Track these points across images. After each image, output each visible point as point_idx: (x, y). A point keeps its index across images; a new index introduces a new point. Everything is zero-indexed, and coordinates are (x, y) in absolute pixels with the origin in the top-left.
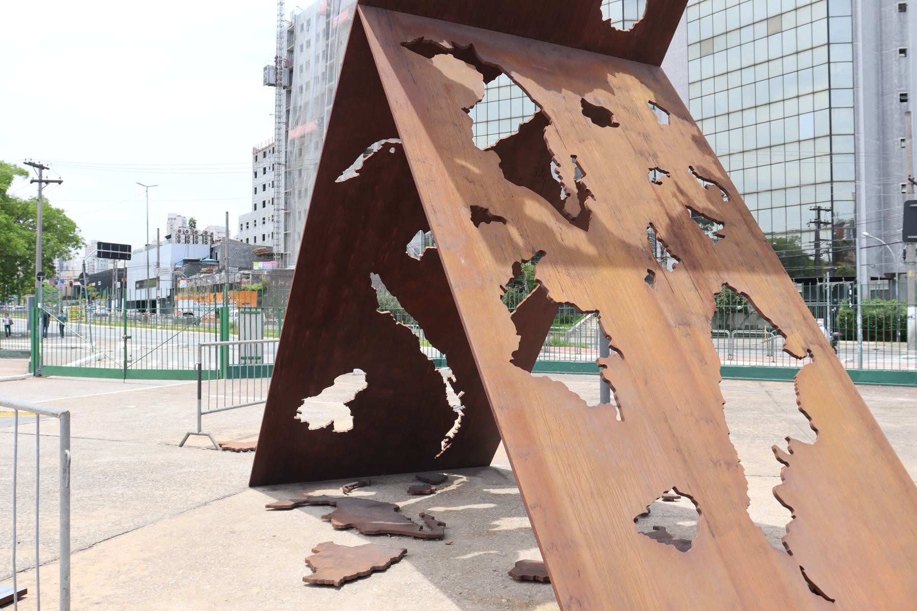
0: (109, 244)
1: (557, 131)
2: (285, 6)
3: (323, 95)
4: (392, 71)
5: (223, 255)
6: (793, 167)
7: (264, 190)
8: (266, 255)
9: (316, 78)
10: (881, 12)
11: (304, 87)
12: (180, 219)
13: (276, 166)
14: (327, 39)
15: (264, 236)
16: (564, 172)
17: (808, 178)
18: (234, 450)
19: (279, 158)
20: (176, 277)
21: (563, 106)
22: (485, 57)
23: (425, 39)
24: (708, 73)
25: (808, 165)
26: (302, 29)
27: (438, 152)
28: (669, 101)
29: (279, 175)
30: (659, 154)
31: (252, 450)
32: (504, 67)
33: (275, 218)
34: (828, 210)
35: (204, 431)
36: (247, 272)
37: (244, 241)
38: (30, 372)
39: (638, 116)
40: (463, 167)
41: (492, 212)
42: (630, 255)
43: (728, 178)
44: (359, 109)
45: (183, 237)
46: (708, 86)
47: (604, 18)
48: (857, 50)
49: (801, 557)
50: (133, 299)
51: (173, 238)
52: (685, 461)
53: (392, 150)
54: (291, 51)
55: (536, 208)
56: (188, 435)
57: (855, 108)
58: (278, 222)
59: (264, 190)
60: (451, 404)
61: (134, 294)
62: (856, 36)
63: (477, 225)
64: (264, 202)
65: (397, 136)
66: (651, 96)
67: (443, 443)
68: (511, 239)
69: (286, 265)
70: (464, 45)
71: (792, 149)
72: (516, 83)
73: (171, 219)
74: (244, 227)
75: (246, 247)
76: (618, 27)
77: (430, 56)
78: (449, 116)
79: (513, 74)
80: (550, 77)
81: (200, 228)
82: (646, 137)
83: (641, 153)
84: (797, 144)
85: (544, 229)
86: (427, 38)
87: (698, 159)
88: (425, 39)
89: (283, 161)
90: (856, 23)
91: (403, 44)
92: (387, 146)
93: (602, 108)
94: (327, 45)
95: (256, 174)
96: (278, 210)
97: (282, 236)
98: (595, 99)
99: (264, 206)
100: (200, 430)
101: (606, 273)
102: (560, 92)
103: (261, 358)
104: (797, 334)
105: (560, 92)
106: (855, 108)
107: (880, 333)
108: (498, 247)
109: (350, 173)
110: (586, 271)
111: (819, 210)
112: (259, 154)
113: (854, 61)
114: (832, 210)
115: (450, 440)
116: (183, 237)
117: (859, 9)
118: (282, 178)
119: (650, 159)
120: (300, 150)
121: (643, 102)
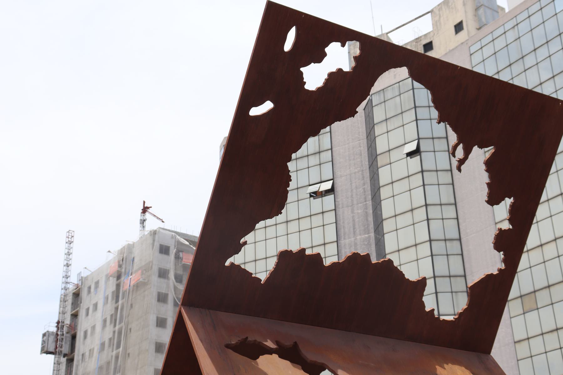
3: (108, 363)
9: (103, 345)
11: (87, 354)
14: (117, 301)
22: (310, 356)
23: (249, 339)
47: (428, 309)
54: (75, 316)
70: (288, 343)
77: (255, 357)
88: (249, 339)
91: (228, 346)
94: (117, 309)
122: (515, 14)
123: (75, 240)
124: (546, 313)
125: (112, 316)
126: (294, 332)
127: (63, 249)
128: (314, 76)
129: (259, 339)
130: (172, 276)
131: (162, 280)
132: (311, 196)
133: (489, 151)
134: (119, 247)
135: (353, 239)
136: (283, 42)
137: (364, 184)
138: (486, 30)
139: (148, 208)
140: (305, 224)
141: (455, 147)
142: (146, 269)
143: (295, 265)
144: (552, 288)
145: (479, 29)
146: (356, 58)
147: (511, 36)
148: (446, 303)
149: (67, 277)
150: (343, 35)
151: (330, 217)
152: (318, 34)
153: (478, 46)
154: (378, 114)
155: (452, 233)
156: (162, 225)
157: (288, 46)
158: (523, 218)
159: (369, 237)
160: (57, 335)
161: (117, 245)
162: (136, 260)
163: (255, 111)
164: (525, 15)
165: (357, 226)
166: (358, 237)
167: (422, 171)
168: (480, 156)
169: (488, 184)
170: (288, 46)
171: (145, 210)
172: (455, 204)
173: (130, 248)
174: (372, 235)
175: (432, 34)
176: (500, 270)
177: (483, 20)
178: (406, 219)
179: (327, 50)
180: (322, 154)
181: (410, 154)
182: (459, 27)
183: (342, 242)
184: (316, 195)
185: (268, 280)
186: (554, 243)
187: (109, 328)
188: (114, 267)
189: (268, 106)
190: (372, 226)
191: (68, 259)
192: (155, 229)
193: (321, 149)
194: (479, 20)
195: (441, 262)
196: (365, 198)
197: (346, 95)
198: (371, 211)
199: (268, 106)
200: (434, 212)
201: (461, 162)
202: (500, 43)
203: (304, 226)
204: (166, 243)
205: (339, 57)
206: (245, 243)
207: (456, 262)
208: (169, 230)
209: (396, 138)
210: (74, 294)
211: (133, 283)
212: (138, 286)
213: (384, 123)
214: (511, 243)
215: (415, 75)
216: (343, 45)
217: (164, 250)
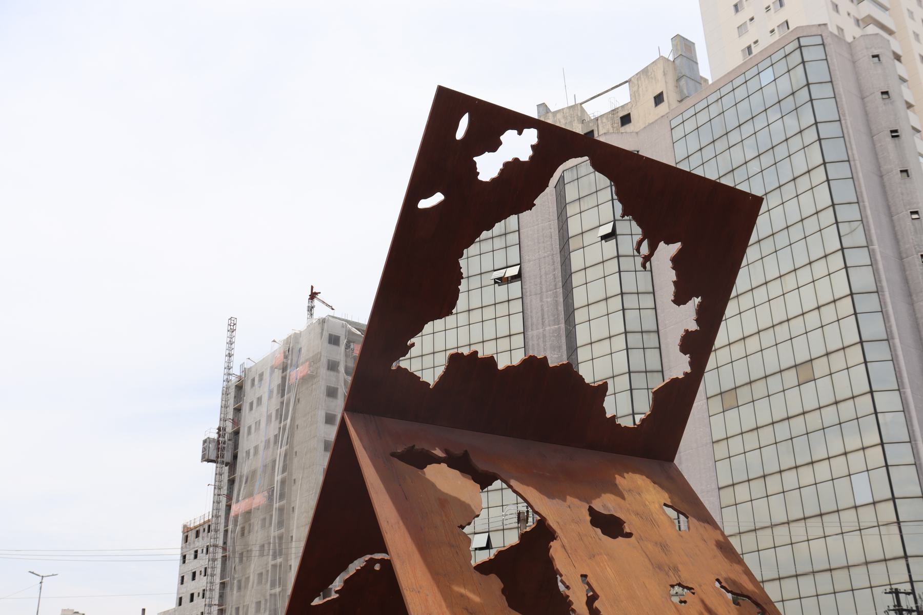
1: (564, 547)
2: (234, 358)
4: (382, 486)
6: (853, 540)
7: (194, 578)
9: (268, 442)
11: (252, 452)
13: (211, 549)
14: (283, 396)
19: (216, 538)
21: (567, 516)
22: (482, 465)
23: (417, 447)
24: (734, 429)
27: (434, 578)
28: (687, 502)
29: (214, 560)
30: (680, 567)
34: (908, 594)
40: (462, 596)
43: (762, 590)
46: (736, 445)
47: (608, 415)
48: (906, 399)
54: (238, 410)
59: (194, 578)
62: (902, 382)
64: (192, 595)
65: (385, 550)
66: (665, 497)
70: (458, 452)
71: (849, 517)
76: (626, 422)
78: (440, 529)
79: (513, 483)
80: (552, 483)
82: (664, 547)
83: (660, 567)
84: (854, 511)
86: (418, 446)
87: (726, 569)
88: (417, 447)
89: (220, 543)
90: (899, 368)
91: (393, 455)
92: (372, 562)
93: (612, 515)
94: (282, 403)
95: (184, 557)
96: (210, 606)
98: (604, 506)
99: (192, 600)
102: (564, 500)
105: (564, 500)
111: (897, 593)
112: (190, 533)
113: (905, 410)
114: (913, 592)
117: (900, 353)
118: (219, 564)
119: (671, 573)
120: (243, 529)
121: (657, 506)
122: (718, 86)
123: (238, 327)
124: (746, 411)
125: (277, 410)
126: (465, 440)
127: (224, 352)
128: (488, 166)
129: (426, 447)
130: (342, 368)
131: (332, 373)
132: (496, 282)
133: (676, 247)
134: (285, 337)
135: (541, 330)
136: (457, 126)
137: (554, 270)
138: (688, 103)
139: (316, 294)
140: (489, 313)
141: (640, 243)
142: (315, 360)
143: (467, 368)
144: (753, 385)
145: (680, 101)
146: (533, 147)
147: (715, 110)
148: (626, 406)
149: (229, 368)
150: (520, 122)
151: (517, 306)
152: (493, 122)
153: (679, 119)
154: (571, 193)
155: (650, 325)
156: (331, 313)
157: (460, 134)
158: (710, 318)
159: (559, 328)
160: (218, 441)
161: (283, 335)
162: (303, 351)
163: (424, 204)
164: (729, 88)
165: (546, 316)
166: (548, 328)
167: (618, 256)
168: (667, 251)
169: (674, 282)
170: (460, 134)
171: (313, 296)
172: (654, 293)
173: (296, 337)
174: (563, 326)
175: (630, 106)
176: (686, 374)
177: (685, 91)
178: (601, 308)
179: (502, 138)
180: (508, 236)
181: (605, 237)
182: (659, 99)
183: (530, 333)
184: (501, 281)
185: (437, 384)
186: (757, 336)
188: (280, 358)
189: (438, 198)
190: (562, 316)
192: (324, 317)
193: (508, 231)
194: (681, 92)
195: (636, 356)
196: (556, 285)
197: (521, 187)
198: (562, 300)
199: (438, 198)
200: (631, 301)
201: (647, 259)
202: (703, 118)
203: (488, 319)
204: (336, 332)
205: (518, 146)
206: (413, 345)
207: (653, 355)
208: (339, 319)
209: (590, 219)
211: (300, 375)
212: (306, 379)
213: (577, 203)
214: (698, 345)
215: (598, 166)
216: (520, 133)
217: (334, 340)
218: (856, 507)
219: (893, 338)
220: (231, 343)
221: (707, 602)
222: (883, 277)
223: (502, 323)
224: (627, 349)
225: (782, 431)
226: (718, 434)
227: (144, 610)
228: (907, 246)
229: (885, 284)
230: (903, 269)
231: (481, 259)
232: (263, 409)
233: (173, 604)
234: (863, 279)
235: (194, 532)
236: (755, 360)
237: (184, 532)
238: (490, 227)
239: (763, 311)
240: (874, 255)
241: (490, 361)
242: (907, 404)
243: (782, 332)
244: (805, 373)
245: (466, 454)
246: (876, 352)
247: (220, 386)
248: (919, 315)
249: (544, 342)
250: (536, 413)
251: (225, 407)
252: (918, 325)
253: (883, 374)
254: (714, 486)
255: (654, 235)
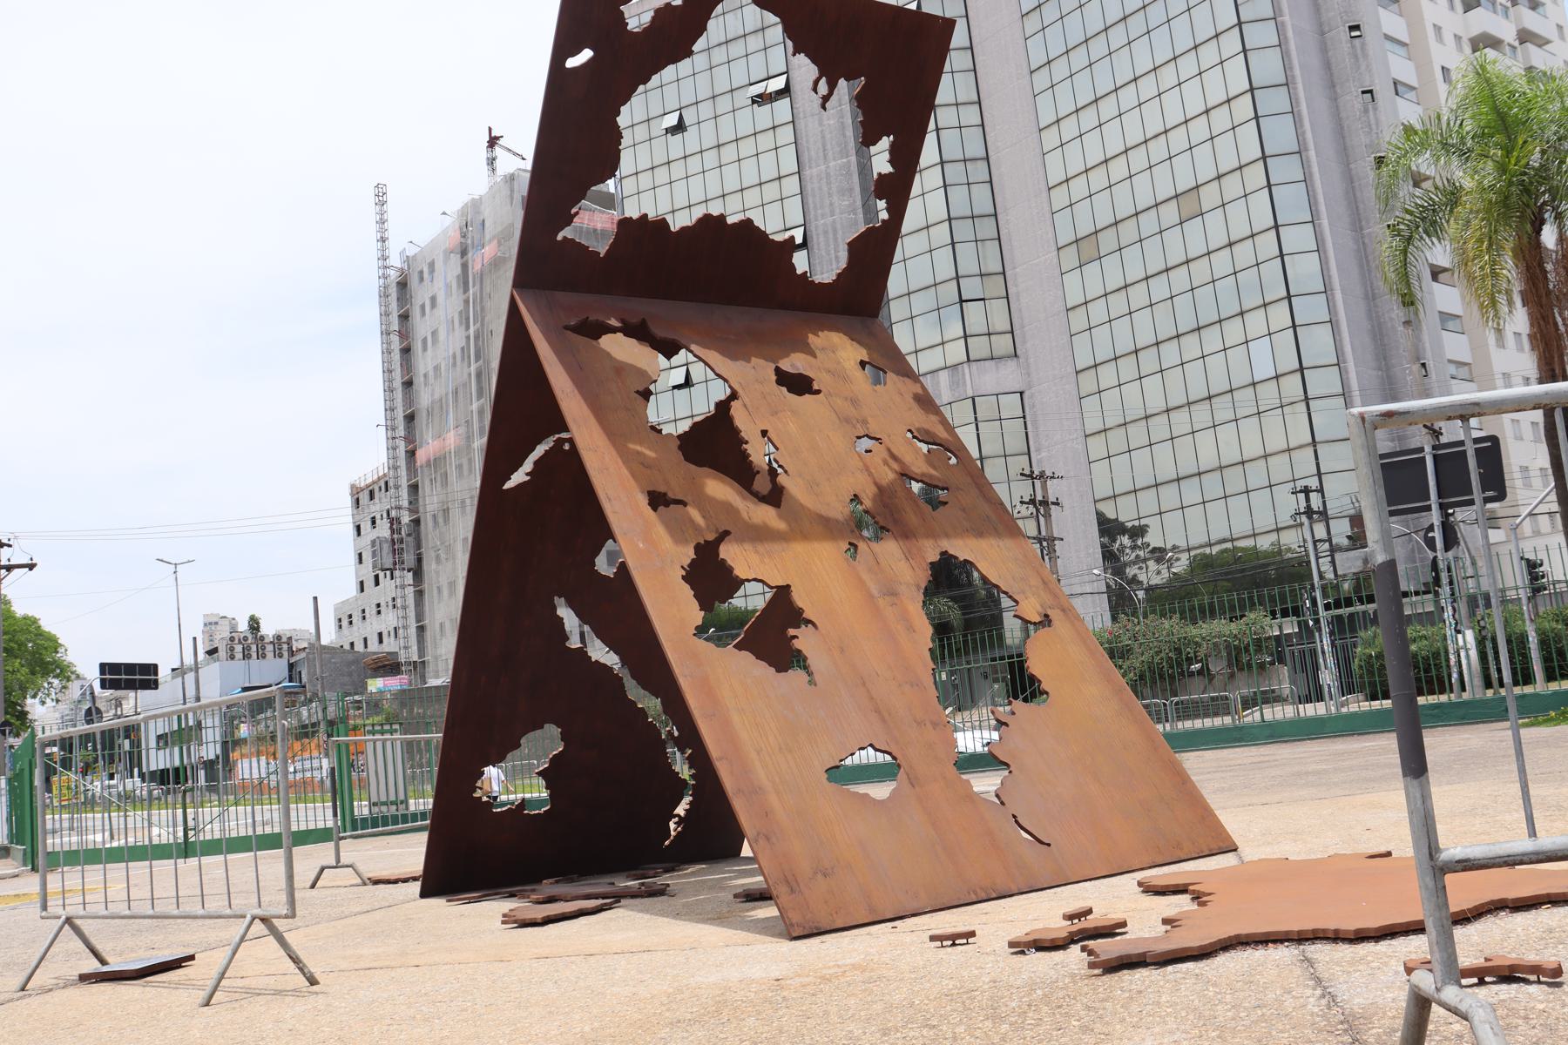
0: (119, 665)
5: (311, 674)
8: (389, 666)
10: (1350, 170)
12: (226, 622)
14: (466, 290)
15: (380, 635)
16: (759, 453)
17: (1276, 442)
18: (389, 882)
20: (233, 718)
21: (753, 376)
22: (659, 332)
24: (1095, 289)
25: (1273, 421)
26: (422, 279)
28: (887, 360)
31: (415, 879)
32: (683, 342)
33: (399, 602)
35: (343, 861)
36: (357, 698)
37: (347, 647)
38: (25, 864)
39: (845, 378)
41: (671, 495)
42: (827, 528)
44: (521, 407)
45: (239, 648)
46: (1098, 311)
49: (1013, 808)
50: (153, 768)
51: (222, 653)
52: (884, 721)
53: (567, 447)
54: (404, 317)
55: (719, 488)
56: (322, 869)
57: (1333, 323)
58: (404, 608)
60: (677, 768)
61: (158, 760)
63: (655, 509)
65: (567, 430)
66: (863, 354)
67: (672, 825)
68: (692, 521)
69: (423, 679)
70: (634, 320)
72: (701, 359)
73: (210, 624)
74: (345, 623)
75: (350, 657)
79: (693, 347)
80: (735, 347)
81: (268, 630)
82: (854, 402)
83: (847, 420)
85: (728, 508)
91: (566, 328)
92: (560, 442)
93: (801, 375)
94: (467, 302)
95: (358, 528)
96: (403, 587)
97: (413, 631)
99: (377, 583)
100: (338, 861)
101: (799, 548)
102: (749, 361)
103: (405, 802)
104: (1033, 600)
105: (749, 361)
106: (1333, 323)
107: (1429, 682)
108: (678, 531)
109: (519, 477)
110: (776, 547)
112: (362, 496)
114: (1321, 490)
115: (681, 820)
116: (239, 648)
123: (390, 197)
124: (1111, 263)
126: (642, 308)
127: (373, 235)
129: (601, 318)
132: (754, 102)
134: (459, 206)
139: (497, 138)
140: (747, 148)
141: (816, 83)
148: (823, 264)
151: (786, 135)
155: (975, 149)
161: (455, 204)
163: (571, 63)
171: (493, 141)
173: (475, 205)
174: (853, 158)
183: (807, 173)
184: (762, 99)
187: (459, 333)
189: (586, 54)
191: (382, 230)
199: (586, 54)
201: (826, 99)
207: (981, 194)
210: (398, 283)
218: (1254, 384)
219: (1307, 150)
220: (382, 222)
221: (895, 451)
222: (1296, 62)
223: (768, 160)
224: (945, 186)
225: (1159, 288)
226: (1074, 298)
227: (315, 599)
228: (1331, 14)
229: (1297, 72)
230: (1324, 49)
231: (641, 115)
232: (440, 311)
233: (353, 590)
234: (1268, 67)
235: (367, 492)
236: (1122, 191)
237: (352, 495)
238: (645, 81)
239: (1132, 119)
240: (1284, 30)
241: (662, 224)
242: (1323, 241)
243: (1158, 149)
244: (1189, 205)
245: (644, 322)
246: (1285, 170)
247: (373, 284)
248: (1343, 115)
249: (829, 183)
250: (719, 276)
251: (385, 314)
252: (1342, 128)
253: (1292, 200)
254: (1071, 370)
255: (830, 71)
